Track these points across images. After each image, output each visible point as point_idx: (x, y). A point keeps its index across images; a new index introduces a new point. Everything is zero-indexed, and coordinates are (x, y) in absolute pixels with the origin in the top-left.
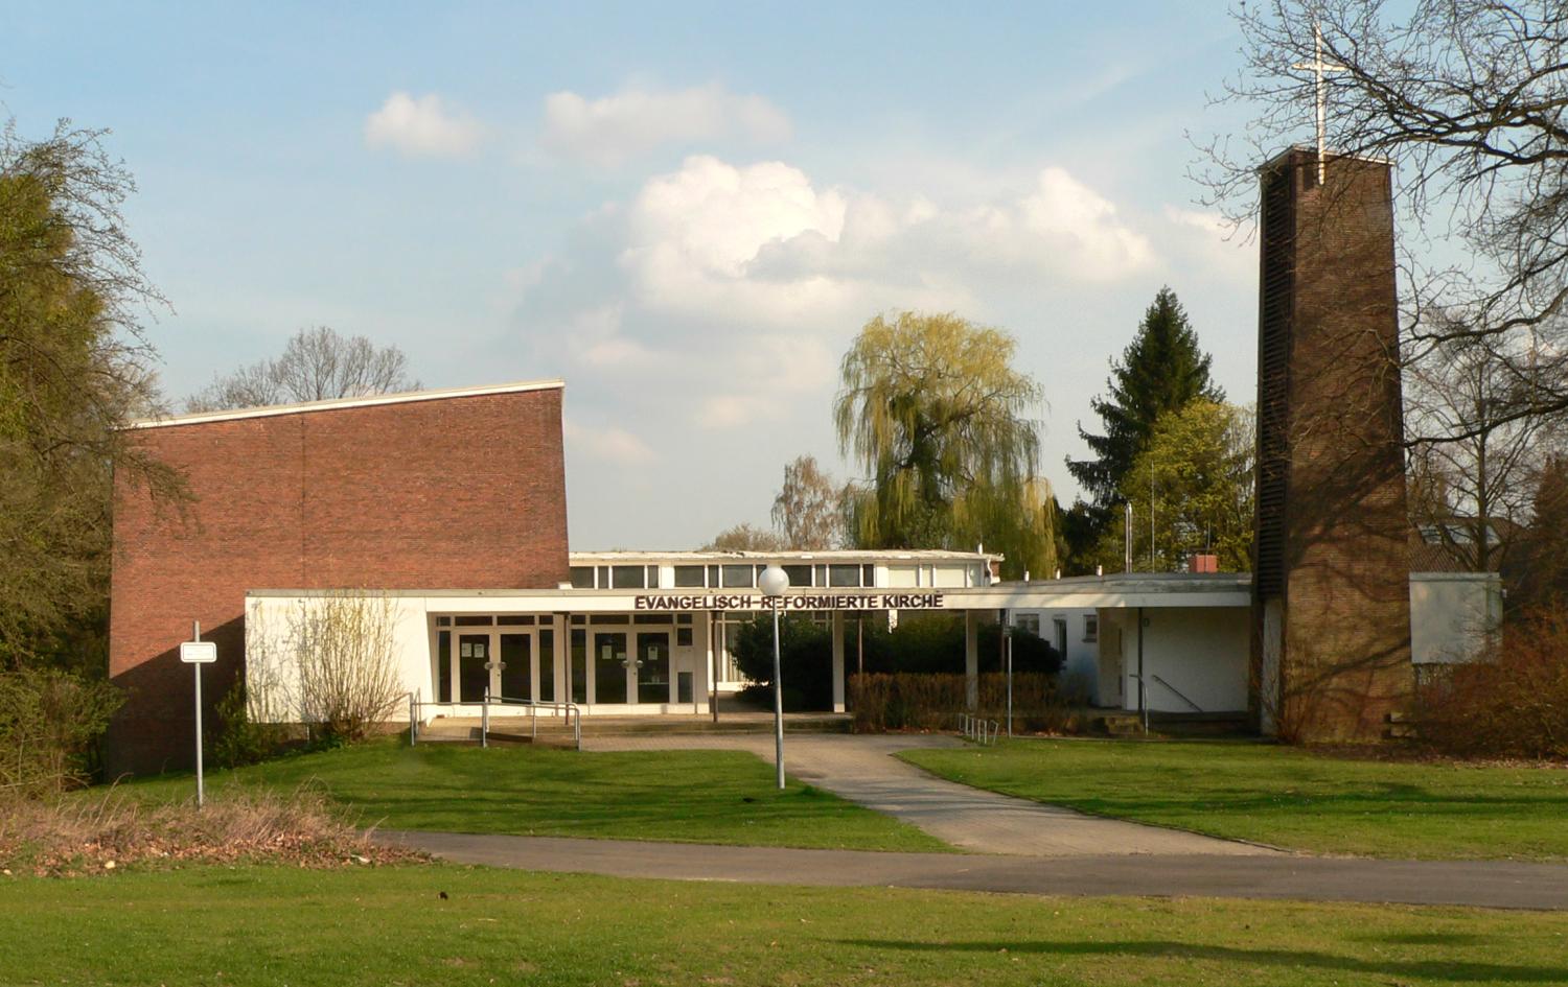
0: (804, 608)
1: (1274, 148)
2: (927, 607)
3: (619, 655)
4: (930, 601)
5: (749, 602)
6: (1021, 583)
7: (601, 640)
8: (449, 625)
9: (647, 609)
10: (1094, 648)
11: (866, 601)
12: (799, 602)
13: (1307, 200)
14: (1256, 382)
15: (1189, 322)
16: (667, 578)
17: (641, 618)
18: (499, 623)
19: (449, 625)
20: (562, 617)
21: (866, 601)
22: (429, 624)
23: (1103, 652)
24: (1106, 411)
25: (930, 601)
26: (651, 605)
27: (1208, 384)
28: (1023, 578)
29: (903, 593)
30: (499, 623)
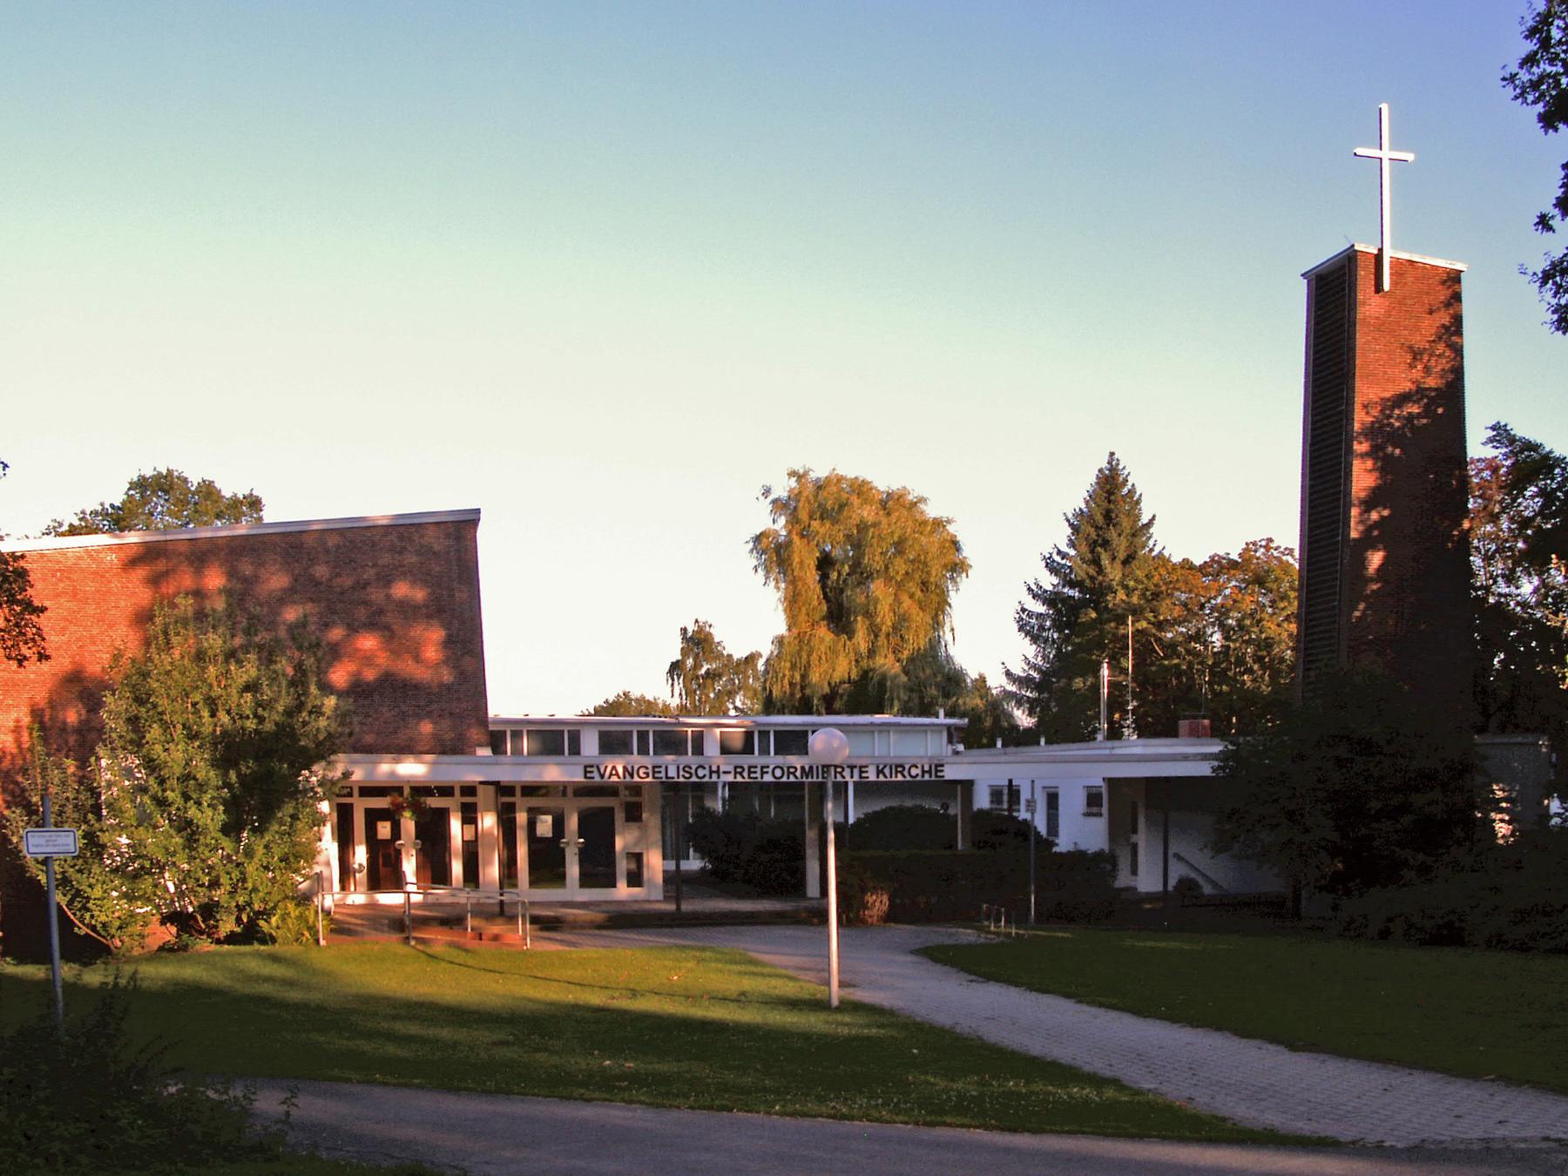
0: (784, 779)
1: (1323, 252)
2: (927, 777)
3: (672, 865)
4: (930, 772)
5: (718, 772)
6: (993, 751)
7: (373, 817)
8: (513, 795)
9: (597, 779)
10: (1100, 825)
11: (856, 771)
12: (778, 773)
13: (1369, 307)
14: (560, 716)
15: (1131, 481)
16: (590, 745)
17: (583, 791)
18: (523, 795)
19: (513, 795)
20: (491, 788)
21: (856, 771)
22: (1308, 322)
23: (1114, 833)
24: (1052, 567)
25: (930, 772)
26: (602, 776)
27: (1151, 543)
28: (995, 745)
29: (899, 762)
30: (523, 795)
